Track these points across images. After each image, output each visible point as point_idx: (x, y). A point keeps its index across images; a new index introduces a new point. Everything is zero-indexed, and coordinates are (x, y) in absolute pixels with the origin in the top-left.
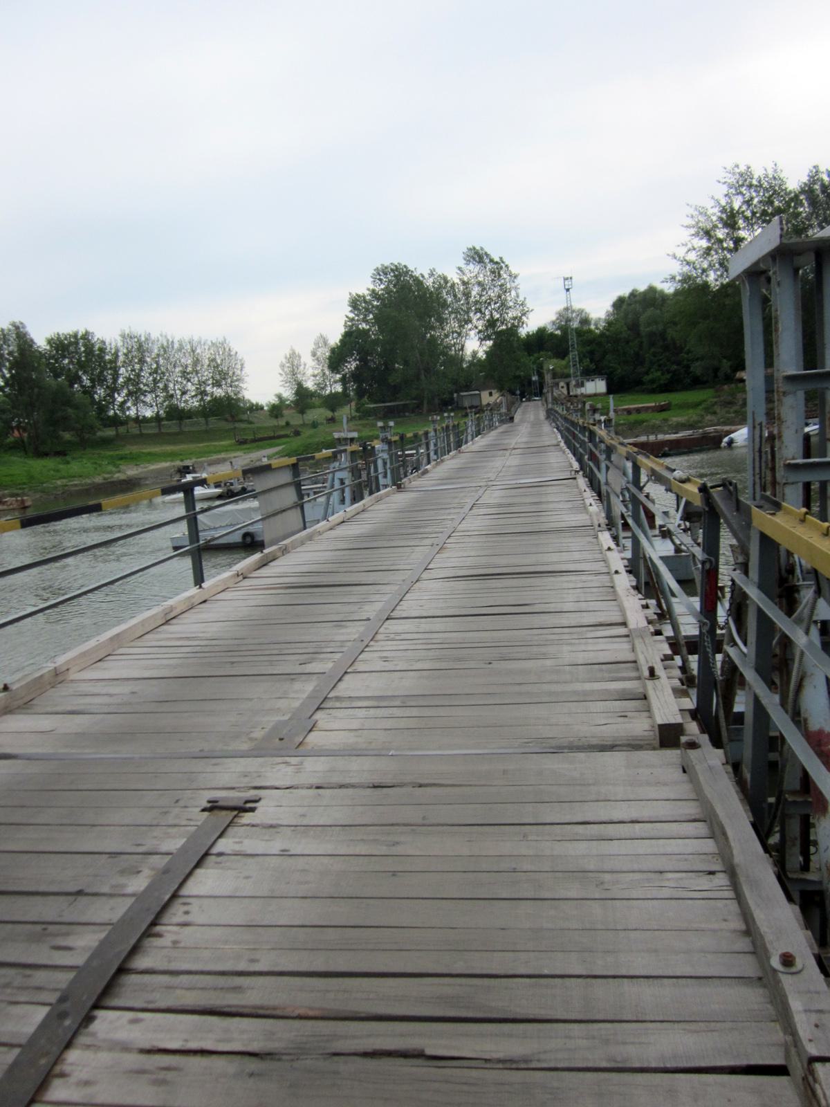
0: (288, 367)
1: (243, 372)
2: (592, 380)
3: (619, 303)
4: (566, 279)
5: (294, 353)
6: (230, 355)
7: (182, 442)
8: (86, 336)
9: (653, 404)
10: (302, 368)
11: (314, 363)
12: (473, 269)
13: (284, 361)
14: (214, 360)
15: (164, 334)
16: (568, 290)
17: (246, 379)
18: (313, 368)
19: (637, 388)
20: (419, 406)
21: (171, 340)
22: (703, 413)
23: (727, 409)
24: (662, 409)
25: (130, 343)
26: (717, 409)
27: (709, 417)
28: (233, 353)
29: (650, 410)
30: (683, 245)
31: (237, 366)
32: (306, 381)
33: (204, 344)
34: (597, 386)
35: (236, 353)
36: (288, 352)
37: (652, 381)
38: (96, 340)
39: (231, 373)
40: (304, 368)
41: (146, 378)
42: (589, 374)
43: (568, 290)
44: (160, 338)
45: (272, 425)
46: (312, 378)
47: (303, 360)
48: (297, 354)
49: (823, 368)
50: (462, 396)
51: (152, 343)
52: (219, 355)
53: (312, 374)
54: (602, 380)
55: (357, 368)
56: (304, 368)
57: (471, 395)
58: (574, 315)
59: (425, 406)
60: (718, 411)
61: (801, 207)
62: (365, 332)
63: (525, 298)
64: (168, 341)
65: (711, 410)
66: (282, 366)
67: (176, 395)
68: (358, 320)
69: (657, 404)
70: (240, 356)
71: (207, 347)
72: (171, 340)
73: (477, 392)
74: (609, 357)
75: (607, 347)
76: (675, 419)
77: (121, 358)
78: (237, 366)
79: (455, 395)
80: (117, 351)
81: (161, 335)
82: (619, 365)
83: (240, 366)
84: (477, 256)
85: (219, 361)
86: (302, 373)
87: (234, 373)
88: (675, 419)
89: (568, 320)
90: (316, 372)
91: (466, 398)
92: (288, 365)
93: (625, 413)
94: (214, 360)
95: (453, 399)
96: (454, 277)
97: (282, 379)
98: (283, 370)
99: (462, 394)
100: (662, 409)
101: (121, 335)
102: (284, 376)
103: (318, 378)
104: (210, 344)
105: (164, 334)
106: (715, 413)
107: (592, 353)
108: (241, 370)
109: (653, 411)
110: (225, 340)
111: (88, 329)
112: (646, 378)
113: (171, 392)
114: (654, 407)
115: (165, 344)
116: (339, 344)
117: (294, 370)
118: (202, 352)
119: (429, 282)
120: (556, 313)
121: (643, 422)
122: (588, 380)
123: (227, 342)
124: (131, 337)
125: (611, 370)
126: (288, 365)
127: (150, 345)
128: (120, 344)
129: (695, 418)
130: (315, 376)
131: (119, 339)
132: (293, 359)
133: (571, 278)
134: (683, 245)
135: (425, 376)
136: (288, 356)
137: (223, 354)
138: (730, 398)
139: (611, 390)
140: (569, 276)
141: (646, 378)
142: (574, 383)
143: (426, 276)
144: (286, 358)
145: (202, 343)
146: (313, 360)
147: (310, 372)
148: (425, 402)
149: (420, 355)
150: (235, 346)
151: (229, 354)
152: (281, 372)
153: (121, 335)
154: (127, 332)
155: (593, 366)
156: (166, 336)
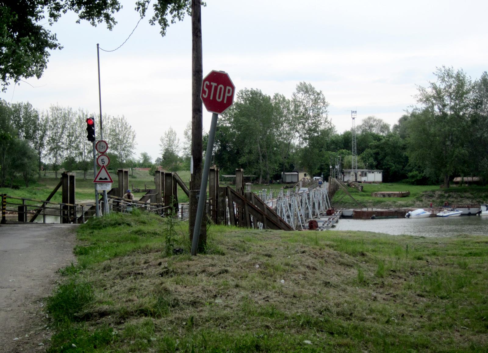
0: (166, 140)
1: (134, 141)
2: (373, 173)
3: (404, 119)
4: (353, 112)
5: (172, 131)
6: (126, 128)
7: (85, 187)
8: (27, 107)
9: (398, 192)
10: (176, 142)
11: (185, 140)
12: (301, 96)
13: (164, 136)
14: (114, 130)
15: (81, 109)
16: (354, 118)
17: (135, 146)
18: (184, 143)
19: (404, 180)
20: (257, 179)
21: (86, 114)
22: (415, 200)
23: (429, 199)
24: (403, 196)
25: (56, 114)
26: (423, 199)
27: (418, 203)
28: (128, 127)
29: (396, 196)
30: (411, 106)
31: (130, 136)
32: (178, 152)
33: (108, 119)
34: (376, 176)
35: (131, 127)
36: (167, 130)
37: (413, 177)
38: (32, 109)
39: (125, 141)
40: (178, 142)
41: (65, 139)
42: (371, 168)
43: (354, 118)
44: (78, 112)
45: (150, 180)
46: (183, 150)
47: (177, 137)
48: (174, 132)
49: (76, 187)
50: (286, 175)
51: (72, 115)
52: (118, 127)
53: (183, 147)
54: (379, 173)
55: (219, 151)
56: (178, 142)
57: (292, 175)
58: (375, 123)
59: (261, 180)
60: (424, 200)
61: (428, 110)
62: (227, 128)
63: (331, 119)
64: (83, 114)
65: (420, 199)
66: (162, 140)
67: (85, 153)
68: (224, 121)
69: (400, 192)
70: (133, 129)
71: (110, 121)
72: (86, 114)
73: (296, 173)
74: (388, 158)
75: (387, 151)
76: (400, 202)
77: (50, 123)
78: (130, 136)
79: (282, 173)
80: (47, 119)
81: (79, 110)
82: (394, 164)
83: (132, 137)
84: (306, 89)
85: (117, 131)
86: (176, 146)
87: (127, 141)
88: (400, 202)
89: (371, 126)
90: (186, 146)
91: (288, 176)
92: (167, 139)
93: (382, 196)
94: (114, 130)
95: (281, 175)
96: (289, 97)
97: (161, 148)
98: (163, 142)
99: (286, 173)
100: (403, 196)
101: (50, 108)
102: (163, 146)
103: (187, 150)
104: (113, 119)
105: (81, 109)
106: (422, 201)
107: (377, 154)
108: (133, 140)
109: (398, 196)
110: (124, 117)
111: (30, 102)
112: (410, 174)
113: (81, 151)
114: (399, 194)
115: (82, 116)
116: (209, 134)
117: (170, 143)
118: (106, 124)
119: (273, 102)
120: (363, 121)
121: (382, 202)
122: (370, 172)
123: (125, 119)
124: (57, 110)
125: (388, 166)
126: (167, 139)
127: (71, 116)
128: (50, 114)
129: (410, 202)
130: (185, 149)
131: (49, 110)
132: (171, 136)
133: (356, 112)
134: (411, 106)
135: (262, 160)
136: (167, 133)
137: (121, 127)
138: (432, 193)
139: (386, 179)
140: (355, 110)
141: (410, 174)
142: (359, 173)
143: (272, 98)
144: (166, 134)
145: (107, 118)
146: (185, 138)
147: (181, 145)
148: (261, 178)
149: (261, 147)
150: (130, 122)
151: (125, 127)
152: (161, 144)
153: (50, 108)
154: (56, 105)
155: (375, 163)
156: (82, 111)
